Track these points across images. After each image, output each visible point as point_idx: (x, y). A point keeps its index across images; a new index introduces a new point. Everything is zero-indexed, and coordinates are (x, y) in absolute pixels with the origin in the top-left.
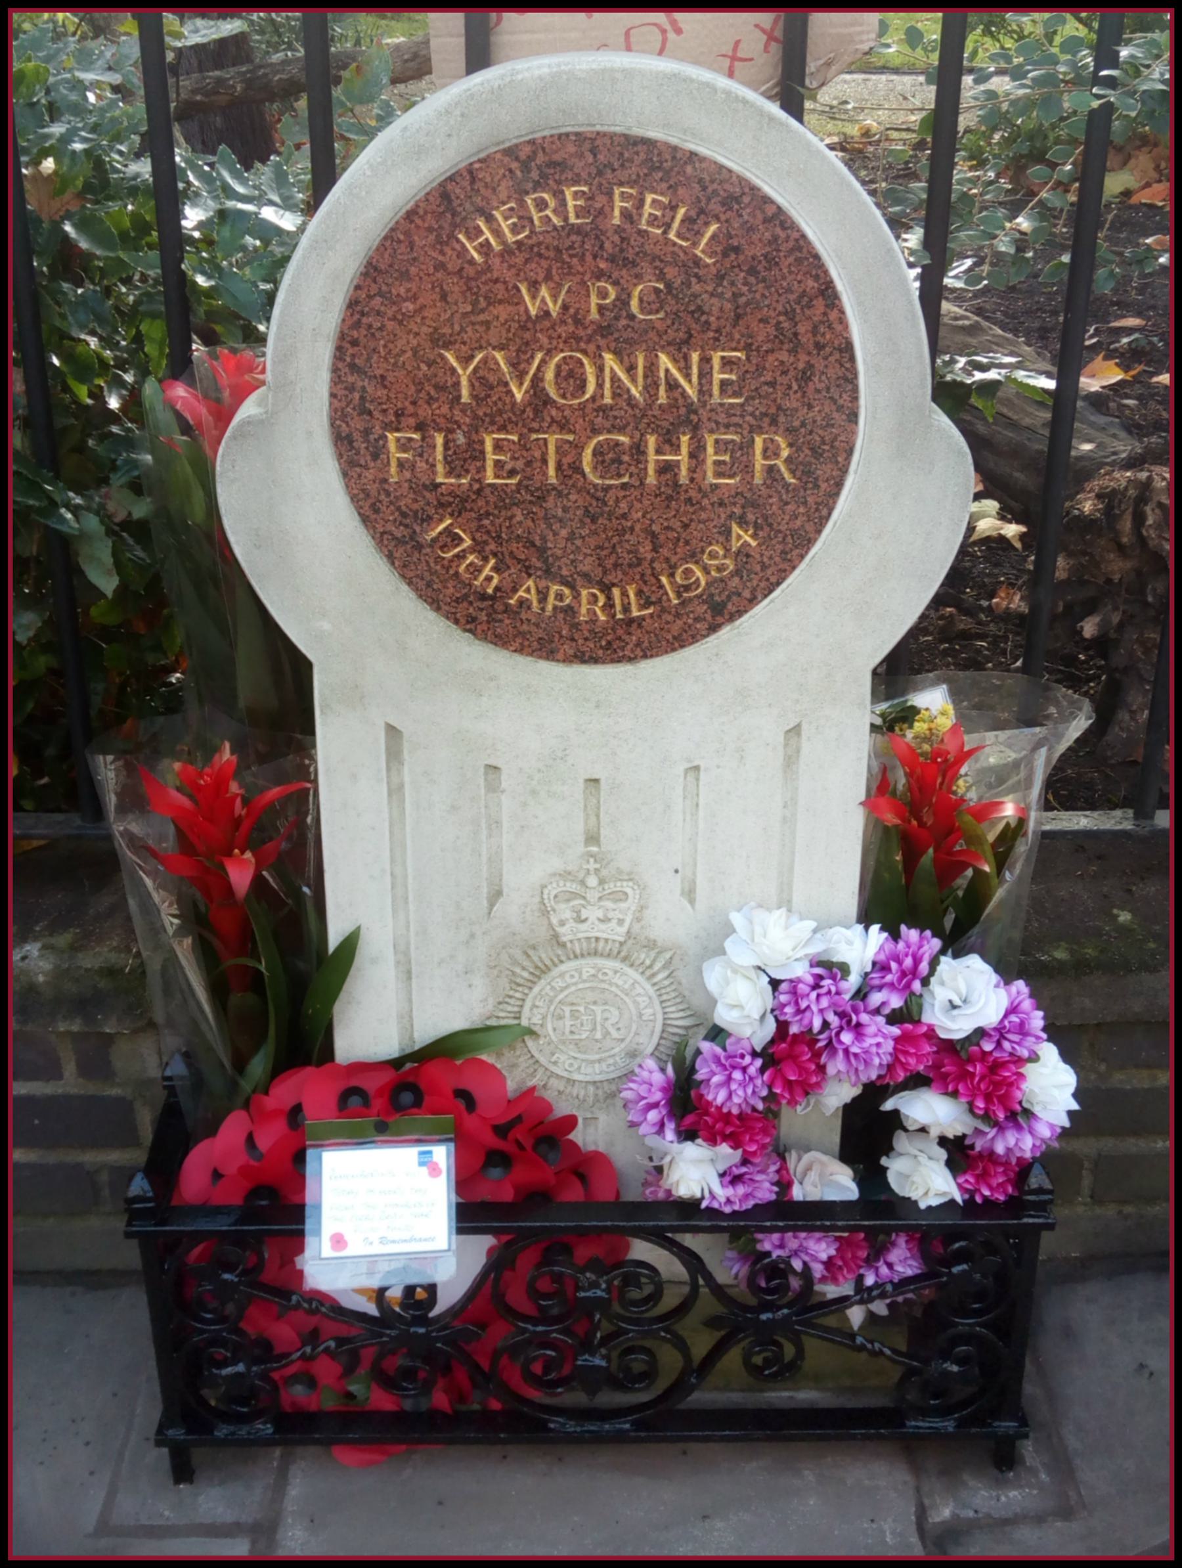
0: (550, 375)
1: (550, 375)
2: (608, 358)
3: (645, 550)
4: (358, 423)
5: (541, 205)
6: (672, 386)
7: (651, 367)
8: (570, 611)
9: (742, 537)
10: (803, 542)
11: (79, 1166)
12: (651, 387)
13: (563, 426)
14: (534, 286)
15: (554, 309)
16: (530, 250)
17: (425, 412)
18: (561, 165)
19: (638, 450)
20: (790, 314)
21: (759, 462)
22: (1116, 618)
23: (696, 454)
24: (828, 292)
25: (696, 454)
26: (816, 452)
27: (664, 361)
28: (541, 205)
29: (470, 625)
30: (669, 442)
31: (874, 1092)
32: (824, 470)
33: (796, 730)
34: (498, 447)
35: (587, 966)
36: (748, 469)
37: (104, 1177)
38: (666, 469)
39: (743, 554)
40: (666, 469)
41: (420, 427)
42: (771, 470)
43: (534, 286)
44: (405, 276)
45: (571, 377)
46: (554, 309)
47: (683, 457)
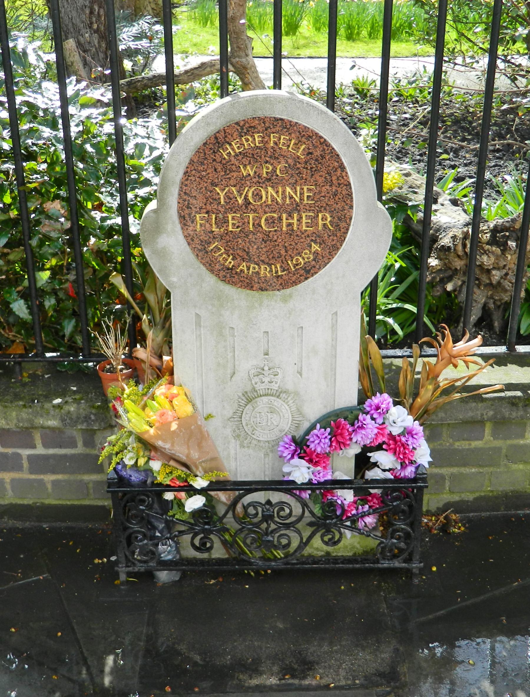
0: (250, 194)
1: (250, 194)
2: (270, 189)
3: (283, 252)
4: (187, 211)
5: (247, 140)
6: (291, 197)
7: (284, 192)
8: (258, 273)
9: (315, 247)
10: (336, 248)
11: (81, 481)
12: (284, 198)
13: (255, 211)
14: (245, 166)
15: (252, 174)
16: (244, 154)
17: (209, 207)
18: (254, 127)
19: (280, 218)
20: (329, 173)
21: (320, 222)
22: (460, 283)
23: (299, 220)
24: (342, 167)
25: (299, 220)
26: (340, 219)
27: (288, 189)
28: (247, 140)
29: (224, 279)
30: (290, 216)
31: (366, 449)
32: (343, 225)
33: (336, 313)
34: (233, 218)
35: (265, 399)
36: (317, 224)
37: (91, 485)
38: (289, 225)
39: (316, 253)
40: (289, 225)
41: (207, 212)
42: (324, 225)
43: (245, 166)
44: (202, 164)
45: (258, 196)
46: (252, 174)
47: (295, 221)
